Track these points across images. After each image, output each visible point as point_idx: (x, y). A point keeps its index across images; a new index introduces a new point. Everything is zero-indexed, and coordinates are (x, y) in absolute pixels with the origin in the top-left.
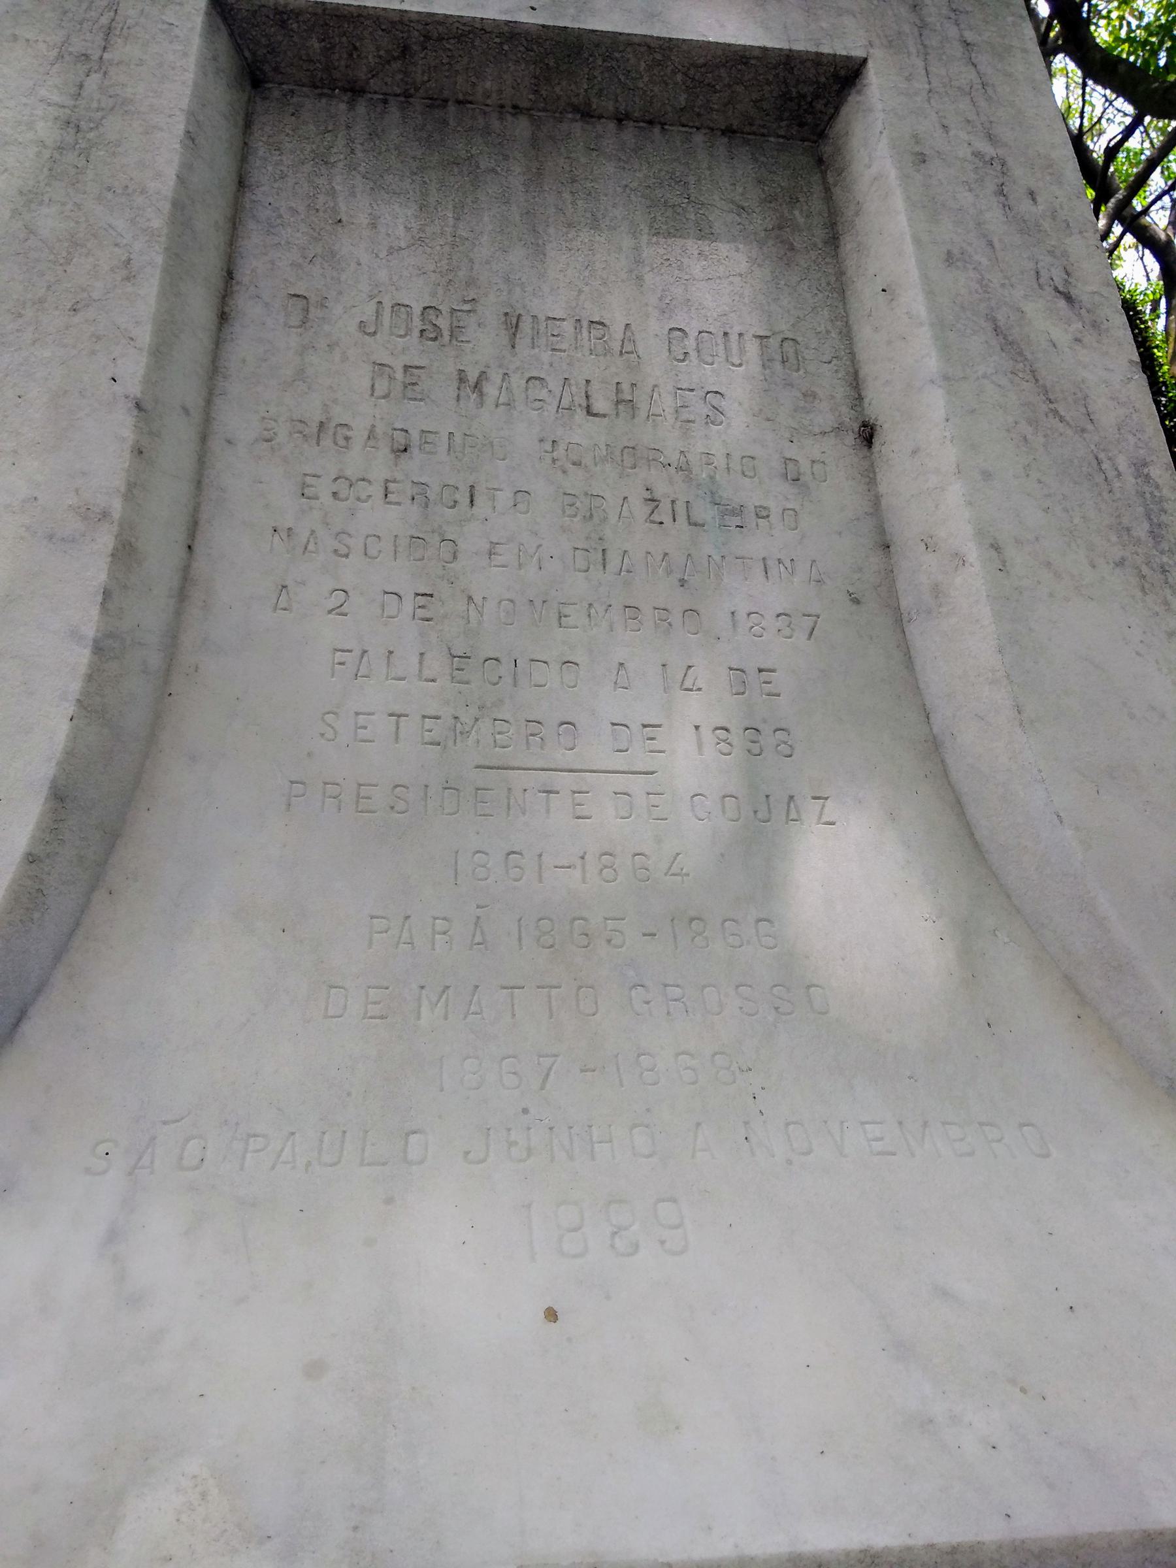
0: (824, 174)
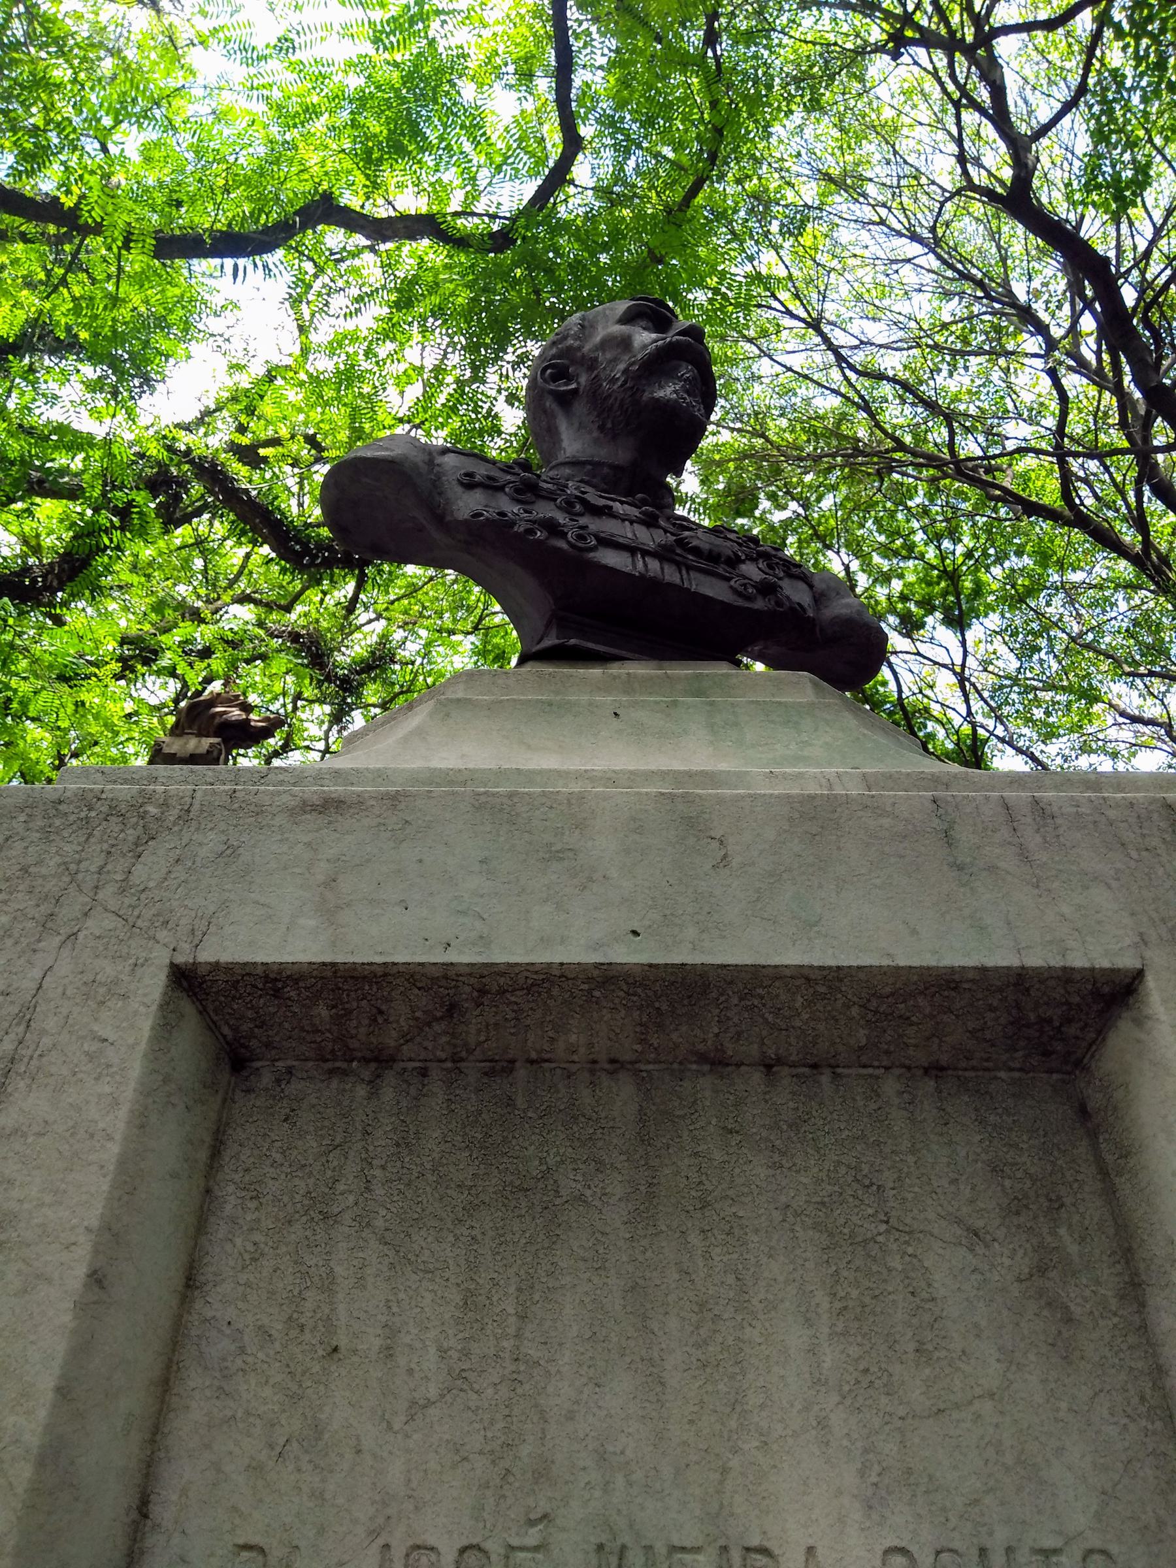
0: (1093, 1135)
